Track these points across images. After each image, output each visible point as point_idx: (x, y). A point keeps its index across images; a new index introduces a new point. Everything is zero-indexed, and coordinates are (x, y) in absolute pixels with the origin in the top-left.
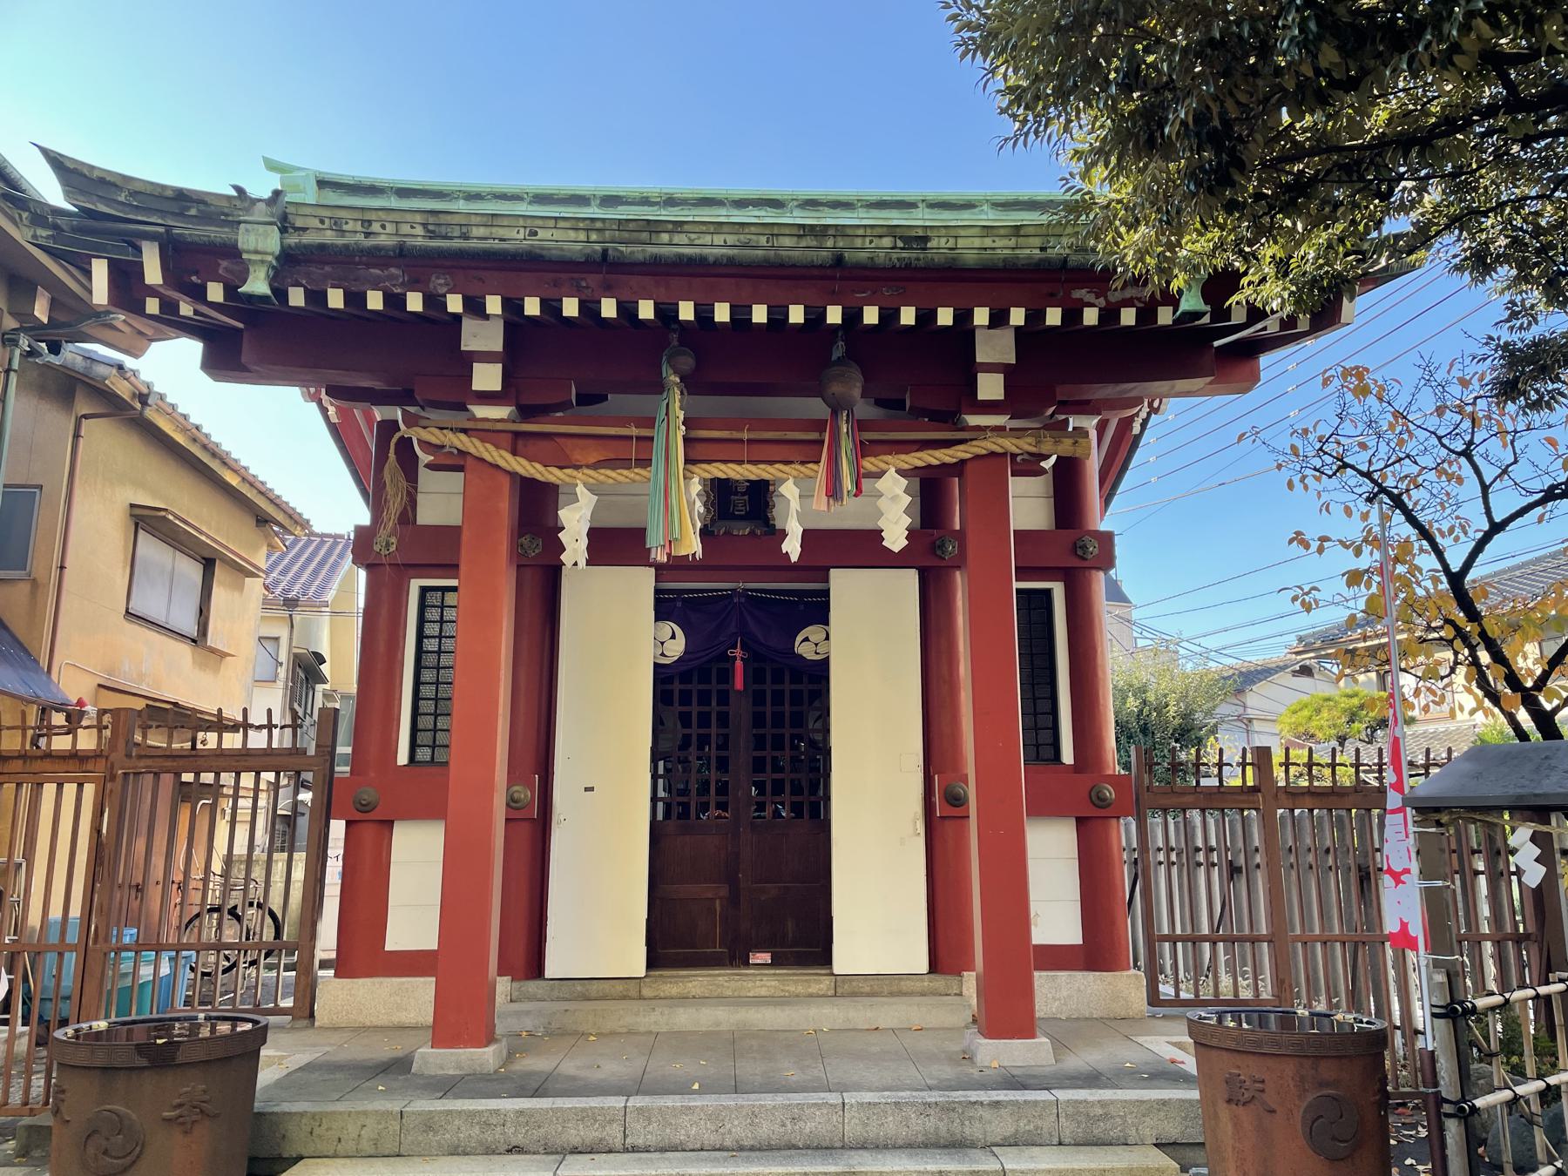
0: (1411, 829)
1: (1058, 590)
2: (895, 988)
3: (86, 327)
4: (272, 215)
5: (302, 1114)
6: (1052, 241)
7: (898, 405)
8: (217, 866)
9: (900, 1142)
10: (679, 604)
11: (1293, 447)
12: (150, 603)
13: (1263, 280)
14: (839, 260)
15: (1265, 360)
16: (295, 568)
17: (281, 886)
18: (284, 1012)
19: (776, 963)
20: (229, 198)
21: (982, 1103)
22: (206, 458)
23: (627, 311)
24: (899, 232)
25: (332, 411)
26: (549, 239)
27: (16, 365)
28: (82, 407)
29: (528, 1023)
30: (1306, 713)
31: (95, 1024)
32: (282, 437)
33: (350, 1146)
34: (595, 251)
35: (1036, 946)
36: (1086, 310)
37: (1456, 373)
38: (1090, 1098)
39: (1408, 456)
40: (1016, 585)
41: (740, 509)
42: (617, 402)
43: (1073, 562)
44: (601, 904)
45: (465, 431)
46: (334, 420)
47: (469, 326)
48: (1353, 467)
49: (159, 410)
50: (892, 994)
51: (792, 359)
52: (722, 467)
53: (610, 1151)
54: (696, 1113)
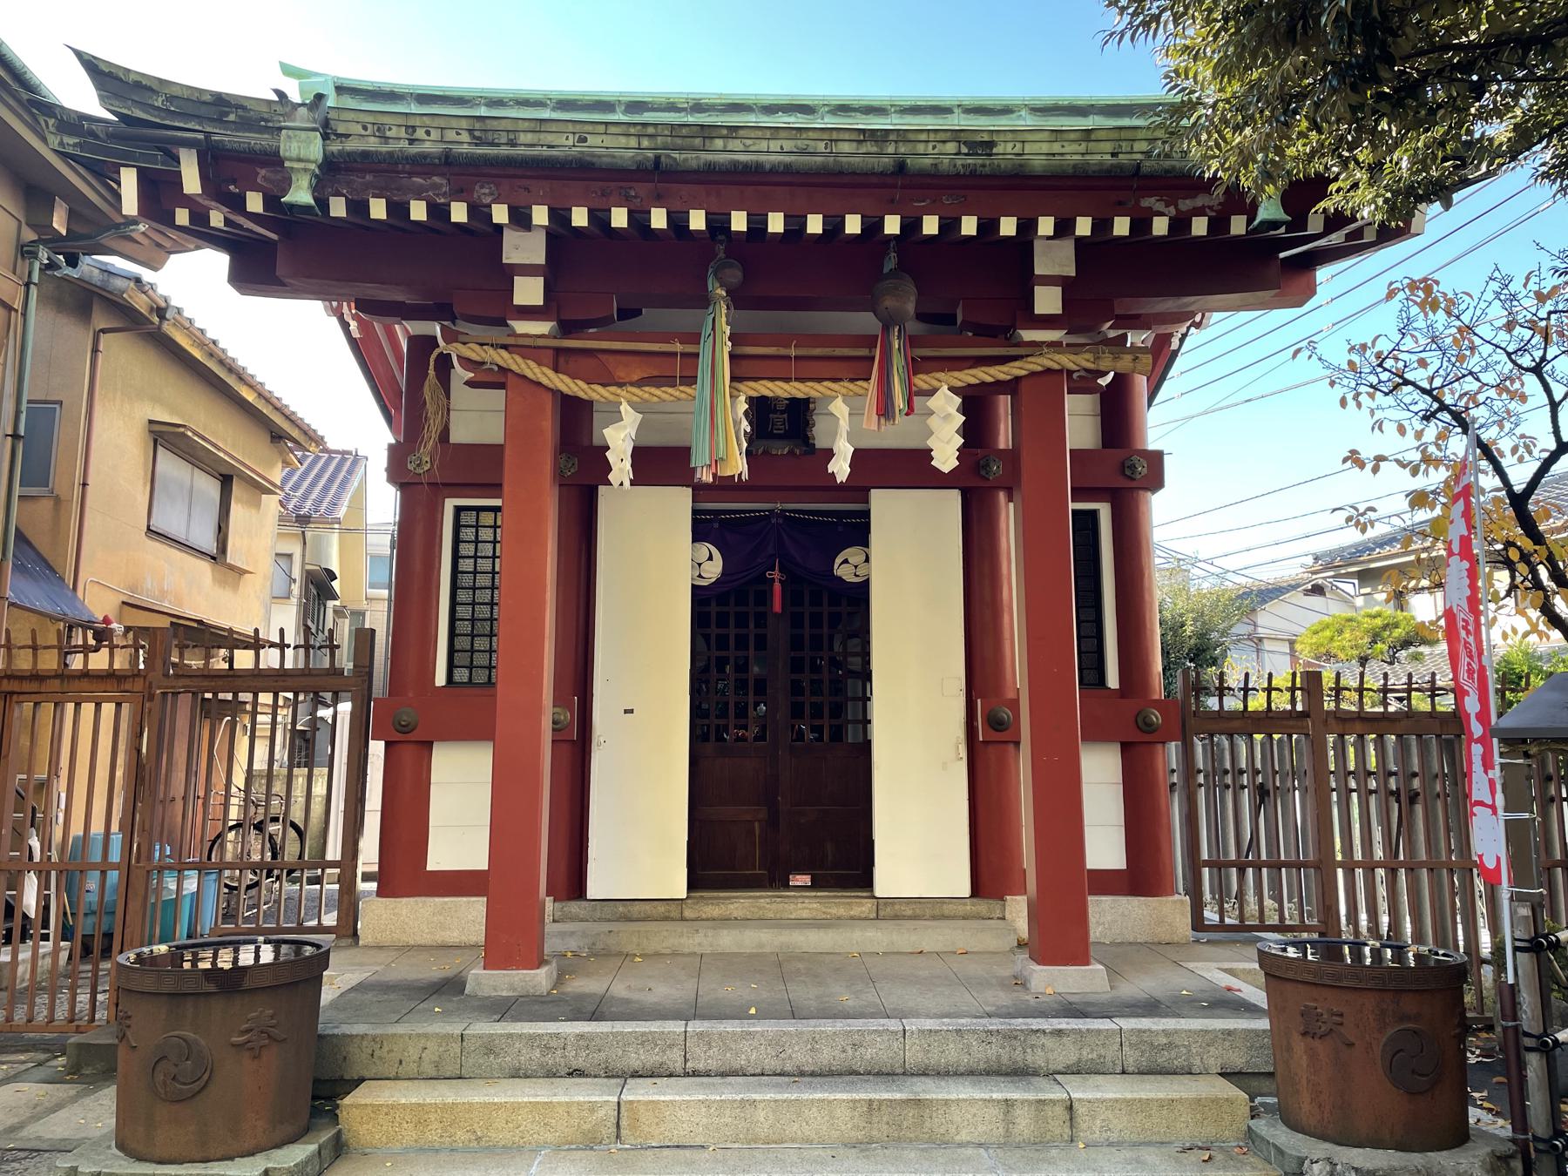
0: (1497, 760)
1: (1104, 511)
2: (937, 912)
3: (106, 240)
4: (315, 121)
5: (363, 1037)
6: (1125, 146)
7: (949, 319)
8: (239, 779)
9: (962, 1069)
10: (716, 525)
11: (1351, 363)
12: (171, 520)
13: (1355, 186)
14: (901, 167)
15: (1322, 273)
16: (306, 484)
17: (301, 800)
18: (328, 930)
19: (816, 885)
20: (269, 102)
21: (1044, 1032)
22: (222, 374)
23: (678, 222)
24: (963, 137)
25: (353, 325)
26: (598, 145)
27: (35, 279)
28: (100, 321)
29: (573, 944)
30: (1328, 633)
31: (155, 948)
32: (302, 352)
33: (411, 1068)
34: (647, 158)
35: (1091, 872)
36: (1156, 219)
37: (1532, 286)
38: (1154, 1028)
39: (1471, 373)
40: (1071, 506)
41: (782, 428)
42: (651, 317)
43: (1122, 483)
44: (641, 831)
45: (505, 347)
46: (356, 334)
47: (511, 238)
48: (1413, 384)
49: (178, 324)
50: (934, 918)
51: (847, 269)
52: (770, 384)
53: (670, 1076)
54: (756, 1039)
